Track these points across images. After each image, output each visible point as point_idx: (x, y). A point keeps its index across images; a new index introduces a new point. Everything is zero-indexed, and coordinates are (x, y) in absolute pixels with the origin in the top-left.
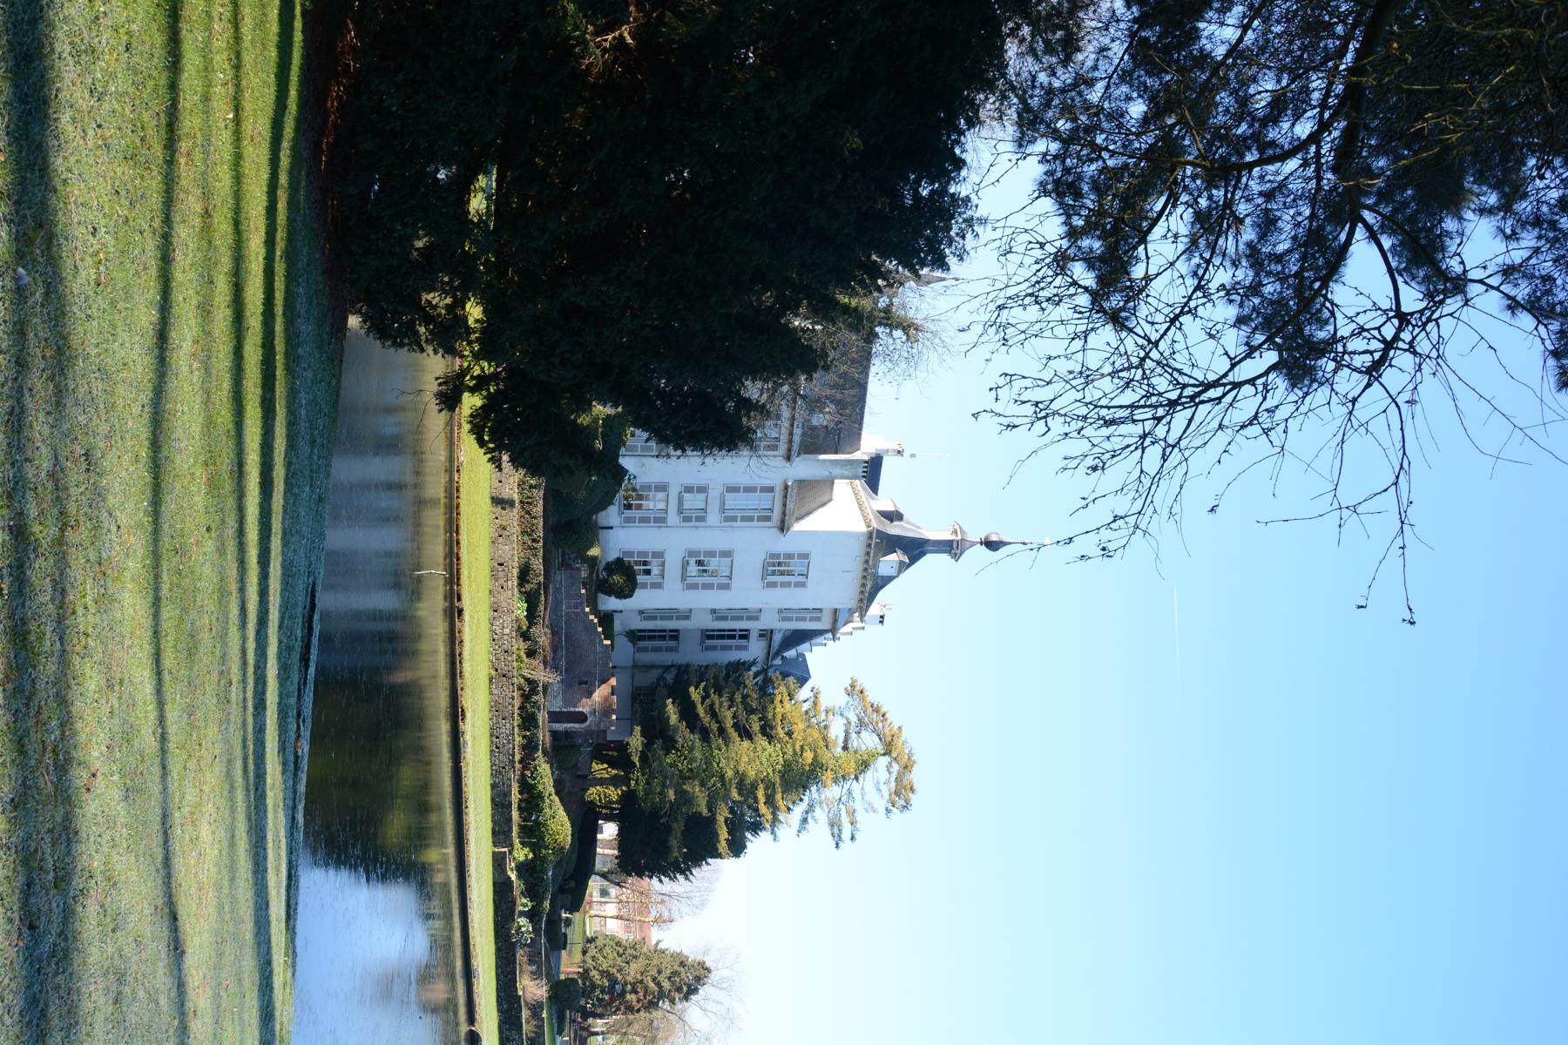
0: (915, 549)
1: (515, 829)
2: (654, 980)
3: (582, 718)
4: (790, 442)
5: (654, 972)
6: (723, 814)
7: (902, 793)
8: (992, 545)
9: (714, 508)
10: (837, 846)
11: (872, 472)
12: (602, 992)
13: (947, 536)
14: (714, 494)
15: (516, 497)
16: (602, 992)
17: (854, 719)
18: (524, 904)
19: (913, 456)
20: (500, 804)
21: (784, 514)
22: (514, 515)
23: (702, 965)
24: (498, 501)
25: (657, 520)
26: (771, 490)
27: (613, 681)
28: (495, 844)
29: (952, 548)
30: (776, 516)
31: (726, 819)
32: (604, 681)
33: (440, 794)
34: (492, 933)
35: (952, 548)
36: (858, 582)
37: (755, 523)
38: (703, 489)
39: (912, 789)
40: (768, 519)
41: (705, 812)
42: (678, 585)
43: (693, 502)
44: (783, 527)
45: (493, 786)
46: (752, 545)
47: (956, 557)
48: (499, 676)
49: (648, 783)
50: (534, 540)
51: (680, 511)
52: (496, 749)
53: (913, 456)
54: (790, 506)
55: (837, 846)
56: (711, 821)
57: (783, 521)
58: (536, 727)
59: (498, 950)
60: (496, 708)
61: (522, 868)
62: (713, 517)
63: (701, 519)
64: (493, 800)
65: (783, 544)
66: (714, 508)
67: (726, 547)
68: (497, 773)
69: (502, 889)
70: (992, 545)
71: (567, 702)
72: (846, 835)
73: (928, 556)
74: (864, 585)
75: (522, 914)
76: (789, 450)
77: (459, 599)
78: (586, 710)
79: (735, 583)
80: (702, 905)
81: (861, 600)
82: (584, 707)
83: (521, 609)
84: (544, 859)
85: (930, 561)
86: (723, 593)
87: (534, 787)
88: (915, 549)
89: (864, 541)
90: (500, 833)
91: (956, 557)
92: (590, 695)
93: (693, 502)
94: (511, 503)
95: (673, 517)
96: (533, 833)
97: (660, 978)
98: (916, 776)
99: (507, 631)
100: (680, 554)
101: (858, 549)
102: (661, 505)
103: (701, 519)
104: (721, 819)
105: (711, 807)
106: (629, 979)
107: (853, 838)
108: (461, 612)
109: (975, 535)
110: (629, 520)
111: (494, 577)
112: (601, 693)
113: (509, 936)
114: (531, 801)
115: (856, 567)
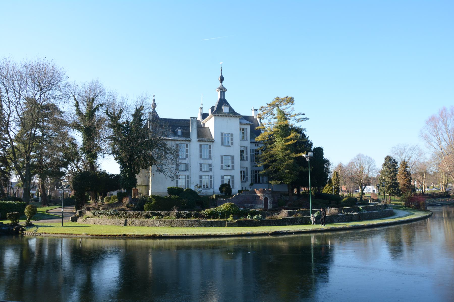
0: (223, 102)
1: (214, 220)
2: (390, 174)
3: (266, 199)
4: (185, 141)
5: (388, 174)
6: (294, 155)
7: (291, 100)
8: (222, 79)
9: (207, 162)
10: (308, 119)
11: (204, 116)
12: (395, 190)
13: (219, 93)
14: (202, 162)
15: (124, 219)
16: (395, 190)
17: (271, 116)
18: (249, 217)
19: (202, 104)
20: (211, 225)
21: (208, 141)
22: (129, 220)
23: (386, 159)
24: (125, 225)
25: (188, 178)
26: (201, 145)
27: (255, 190)
28: (224, 226)
29: (223, 91)
30: (209, 143)
31: (296, 153)
32: (255, 193)
33: (180, 242)
34: (242, 228)
35: (223, 91)
36: (231, 118)
37: (189, 149)
38: (201, 165)
39: (287, 97)
40: (210, 146)
41: (292, 160)
42: (233, 171)
43: (205, 168)
44: (212, 141)
45: (205, 226)
46: (218, 150)
47: (226, 90)
48: (171, 225)
49: (287, 178)
50: (139, 214)
51: (208, 172)
52: (193, 226)
53: (202, 104)
54: (206, 139)
55: (308, 119)
56: (296, 158)
57: (211, 141)
58: (191, 213)
59: (263, 225)
60: (180, 226)
61: (234, 218)
62: (210, 162)
63: (210, 165)
64: (209, 227)
65: (218, 140)
66: (207, 162)
67: (220, 158)
68: (201, 225)
69: (240, 224)
70: (222, 79)
71: (261, 204)
72: (303, 117)
73: (225, 98)
74: (231, 116)
75: (252, 217)
76: (188, 141)
77: (120, 235)
78: (263, 198)
79: (231, 154)
80: (371, 159)
81: (236, 117)
82: (262, 198)
83: (154, 218)
84: (234, 211)
85: (227, 97)
86: (235, 158)
87: (209, 214)
88: (223, 102)
89: (217, 117)
90: (221, 225)
91: (226, 90)
92: (259, 197)
93: (205, 168)
94: (126, 220)
95: (210, 173)
96: (225, 214)
97: (389, 171)
98: (283, 96)
99: (159, 222)
100: (222, 171)
101: (220, 119)
102: (207, 177)
103: (210, 165)
104: (295, 155)
105: (290, 158)
106: (390, 181)
107: (304, 114)
108: (124, 235)
109: (219, 85)
110: (211, 186)
111: (144, 226)
112: (258, 194)
113: (258, 222)
114: (214, 215)
115: (226, 119)
